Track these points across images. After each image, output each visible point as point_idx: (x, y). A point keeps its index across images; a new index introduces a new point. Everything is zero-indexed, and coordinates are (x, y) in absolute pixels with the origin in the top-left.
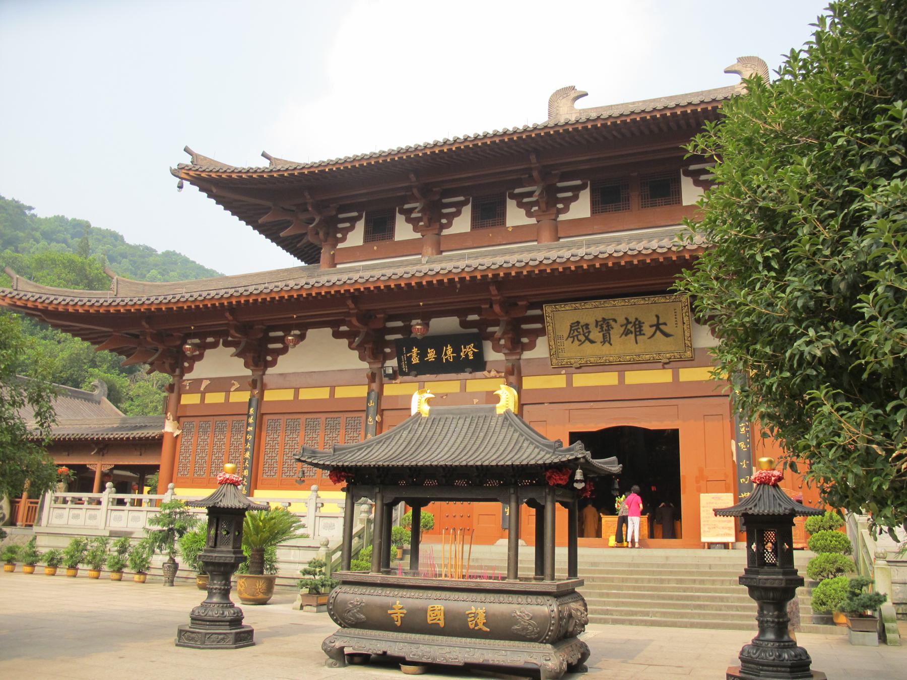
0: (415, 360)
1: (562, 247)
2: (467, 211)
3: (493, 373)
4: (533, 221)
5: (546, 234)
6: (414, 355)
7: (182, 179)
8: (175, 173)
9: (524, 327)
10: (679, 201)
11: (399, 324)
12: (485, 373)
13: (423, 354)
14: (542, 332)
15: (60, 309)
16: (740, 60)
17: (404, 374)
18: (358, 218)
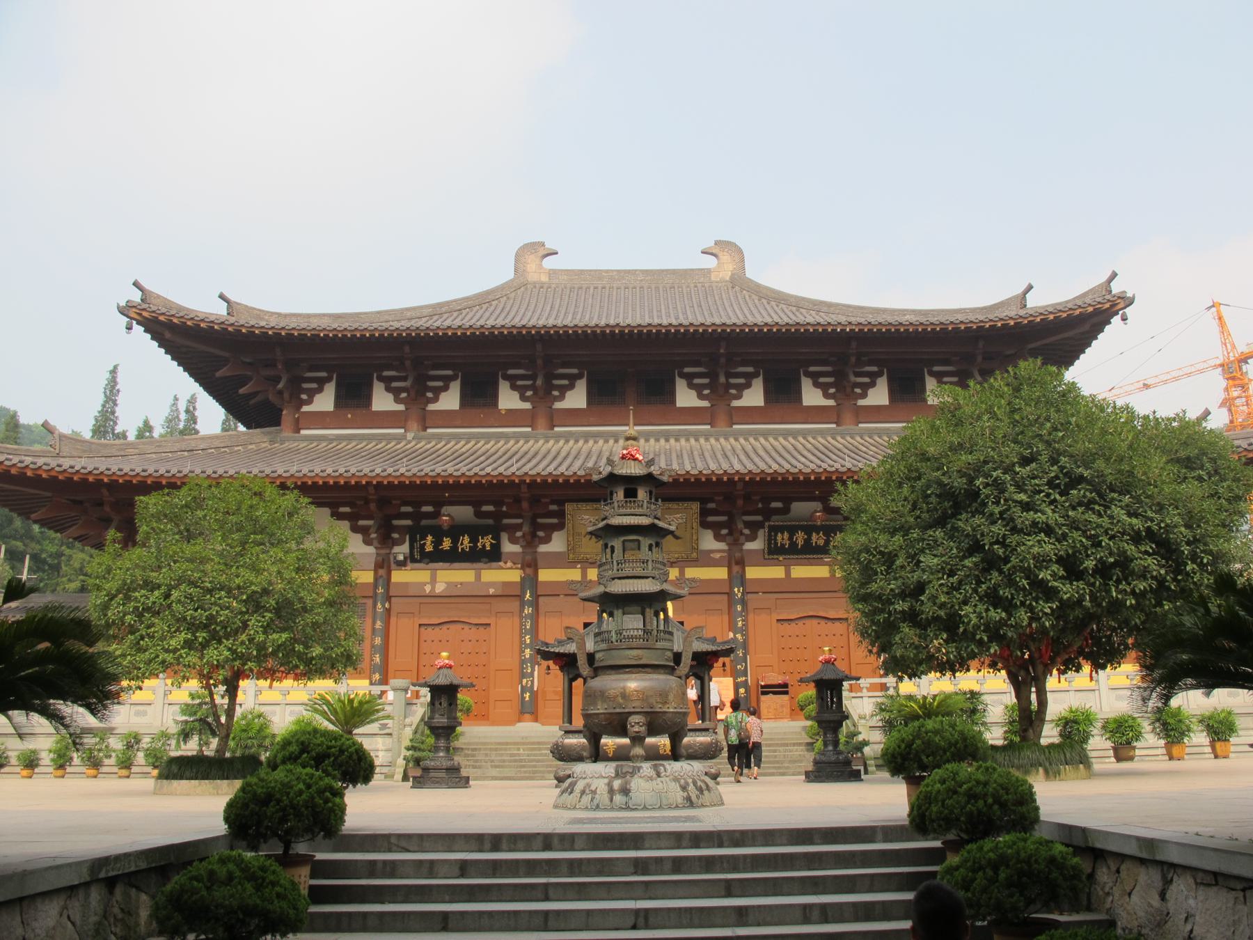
0: (429, 548)
1: (558, 437)
2: (455, 387)
3: (509, 564)
4: (527, 406)
5: (541, 422)
6: (428, 543)
7: (132, 318)
8: (123, 311)
9: (540, 520)
10: (673, 402)
11: (409, 509)
12: (501, 564)
13: (437, 543)
14: (560, 526)
15: (13, 471)
16: (717, 243)
17: (414, 560)
18: (329, 380)
